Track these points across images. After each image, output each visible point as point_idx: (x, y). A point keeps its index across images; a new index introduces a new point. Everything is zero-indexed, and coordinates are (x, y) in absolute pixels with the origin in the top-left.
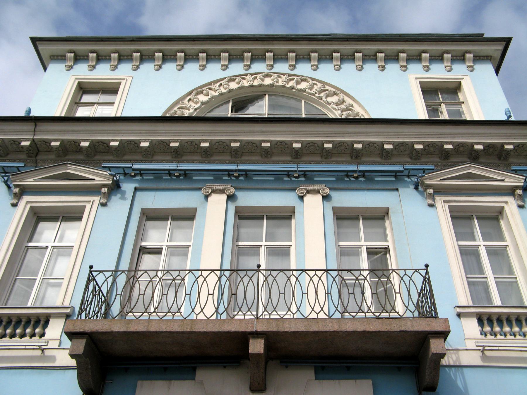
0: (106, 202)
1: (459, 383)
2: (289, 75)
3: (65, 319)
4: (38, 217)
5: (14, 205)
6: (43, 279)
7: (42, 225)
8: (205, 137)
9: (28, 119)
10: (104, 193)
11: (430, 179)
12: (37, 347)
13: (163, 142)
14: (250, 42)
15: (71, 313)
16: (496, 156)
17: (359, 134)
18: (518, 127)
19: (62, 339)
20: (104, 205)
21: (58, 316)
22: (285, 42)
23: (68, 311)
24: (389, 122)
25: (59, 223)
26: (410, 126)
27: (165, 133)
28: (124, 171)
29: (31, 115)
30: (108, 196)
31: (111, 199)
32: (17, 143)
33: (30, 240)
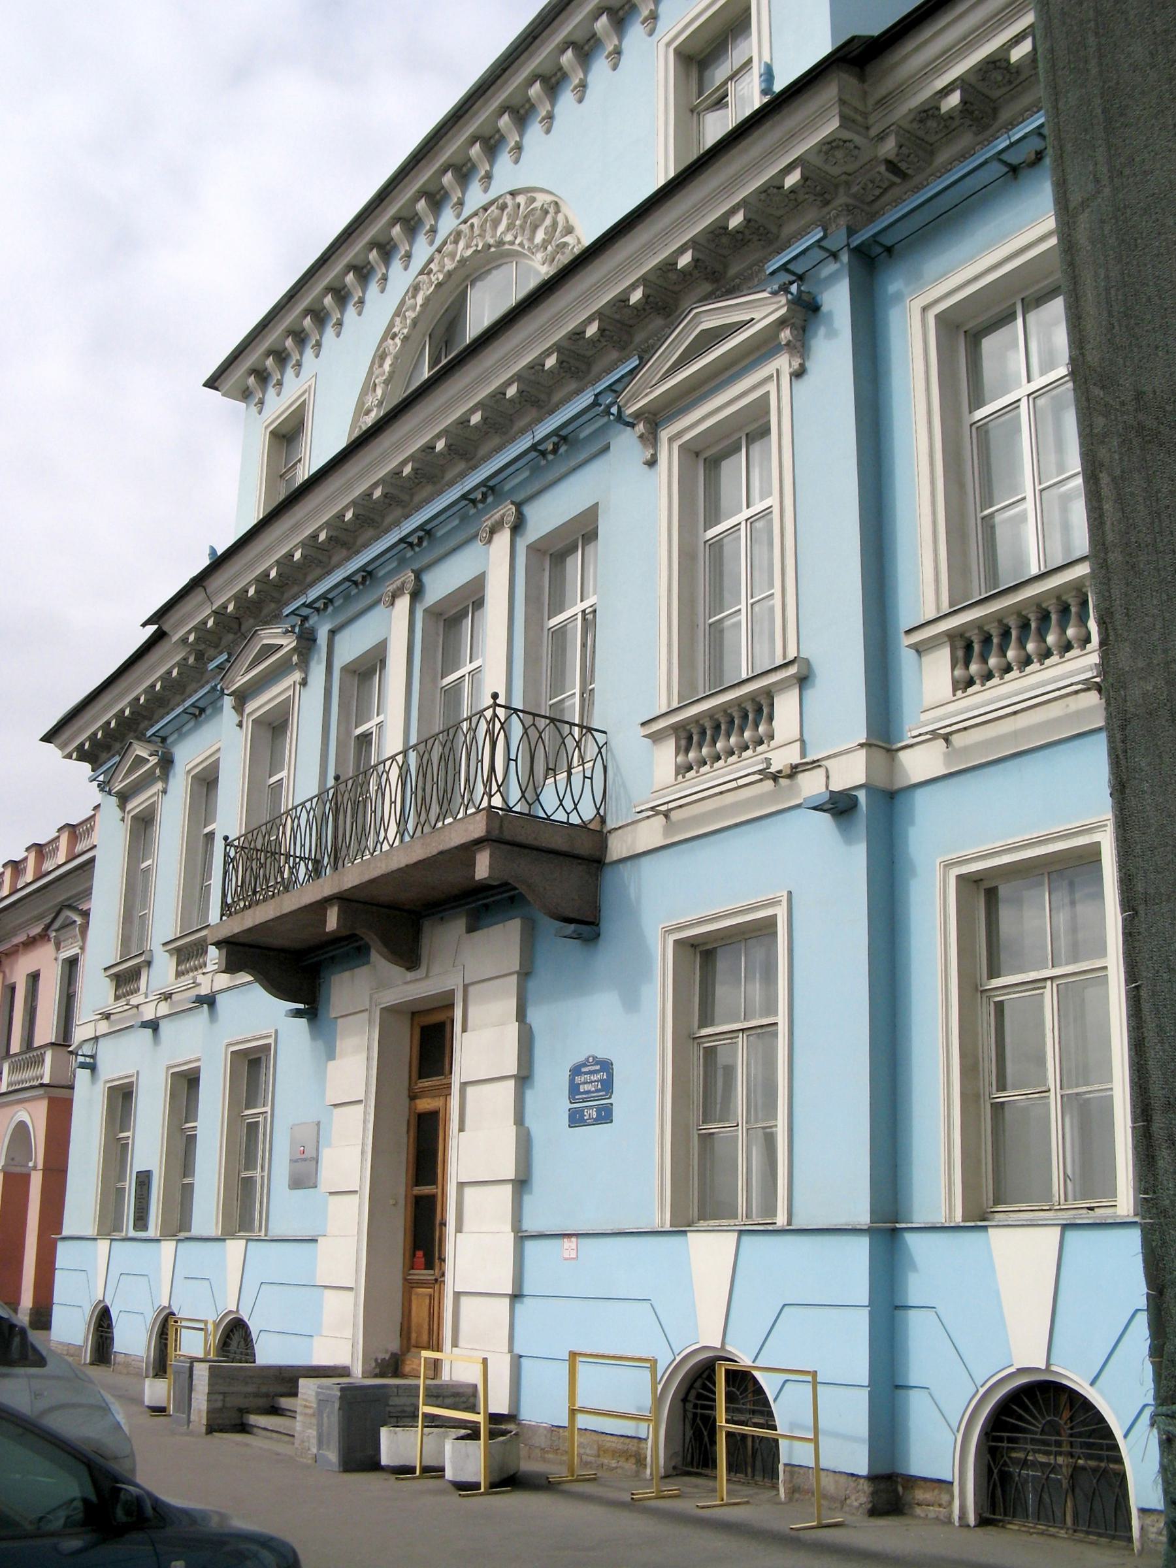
0: (802, 366)
1: (626, 874)
2: (439, 251)
3: (797, 690)
4: (708, 459)
5: (652, 463)
6: (1041, 491)
7: (989, 344)
8: (426, 430)
9: (219, 562)
10: (788, 344)
11: (634, 397)
12: (1080, 687)
13: (764, 190)
14: (523, 58)
15: (804, 672)
16: (721, 264)
17: (620, 271)
18: (734, 152)
19: (805, 737)
20: (799, 374)
21: (783, 685)
22: (454, 129)
23: (793, 670)
24: (529, 306)
25: (1020, 321)
26: (424, 403)
27: (650, 247)
28: (826, 250)
29: (219, 553)
30: (801, 347)
31: (809, 349)
32: (722, 231)
33: (977, 401)
